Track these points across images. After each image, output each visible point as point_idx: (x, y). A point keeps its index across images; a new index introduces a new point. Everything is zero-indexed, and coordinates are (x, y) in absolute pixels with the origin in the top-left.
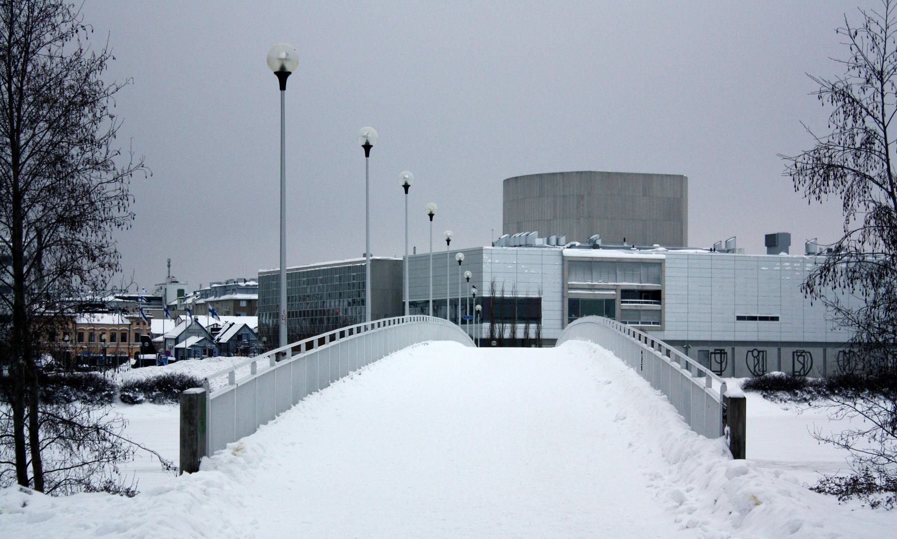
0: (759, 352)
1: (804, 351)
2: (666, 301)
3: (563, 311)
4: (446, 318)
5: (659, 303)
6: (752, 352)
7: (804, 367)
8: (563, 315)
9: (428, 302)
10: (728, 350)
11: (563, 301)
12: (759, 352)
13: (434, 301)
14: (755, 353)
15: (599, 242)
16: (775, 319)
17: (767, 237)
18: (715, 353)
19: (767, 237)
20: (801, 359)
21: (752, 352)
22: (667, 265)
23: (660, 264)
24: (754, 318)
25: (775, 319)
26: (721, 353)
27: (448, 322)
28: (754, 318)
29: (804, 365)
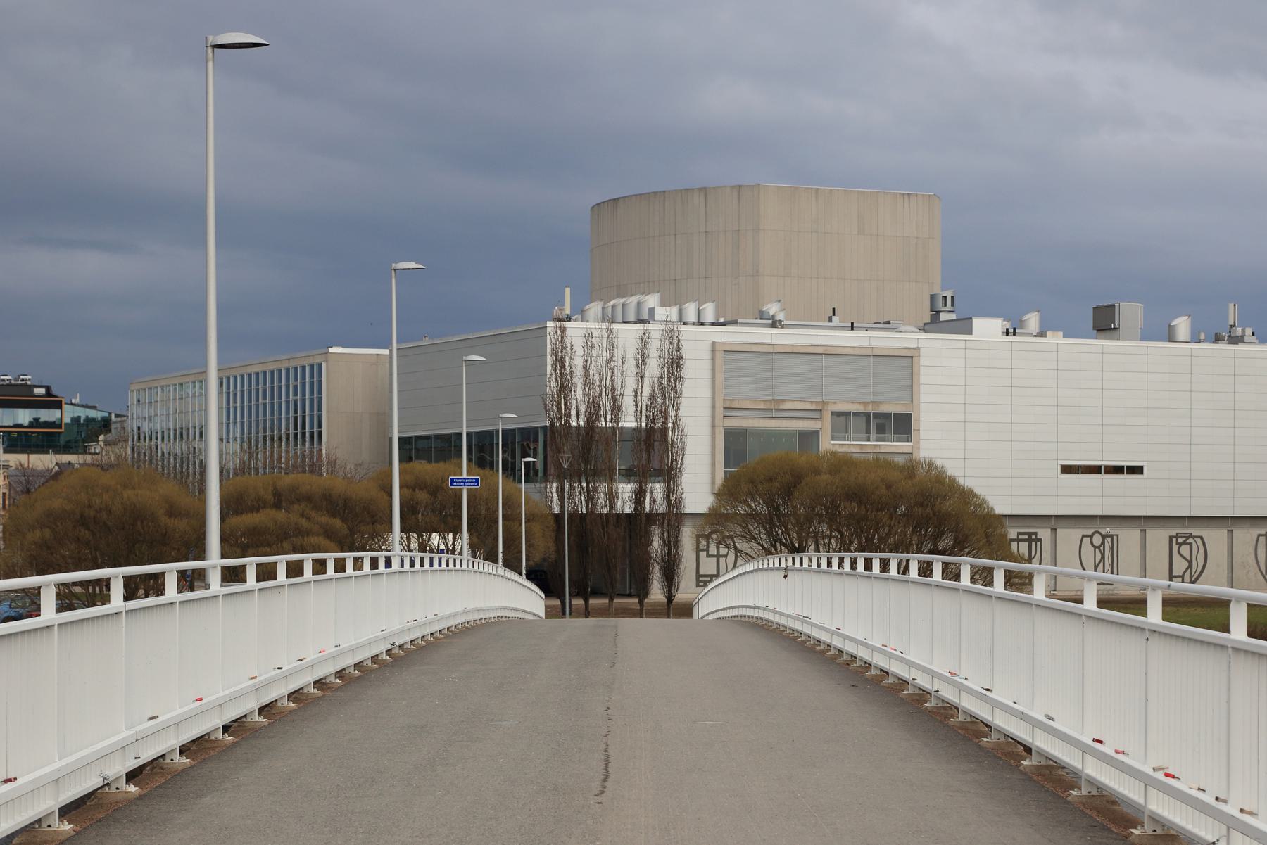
0: (1104, 537)
1: (1191, 536)
2: (923, 435)
3: (713, 455)
4: (496, 561)
5: (909, 440)
6: (1091, 537)
7: (1190, 567)
8: (713, 464)
9: (461, 434)
10: (1044, 533)
11: (713, 435)
12: (1104, 537)
13: (468, 434)
14: (1097, 540)
15: (780, 317)
16: (1137, 470)
17: (1097, 310)
18: (1018, 540)
19: (1097, 310)
20: (1185, 550)
21: (1091, 537)
22: (923, 361)
23: (909, 359)
24: (1095, 470)
25: (1137, 470)
26: (1029, 541)
27: (500, 570)
28: (1095, 470)
29: (1190, 562)
